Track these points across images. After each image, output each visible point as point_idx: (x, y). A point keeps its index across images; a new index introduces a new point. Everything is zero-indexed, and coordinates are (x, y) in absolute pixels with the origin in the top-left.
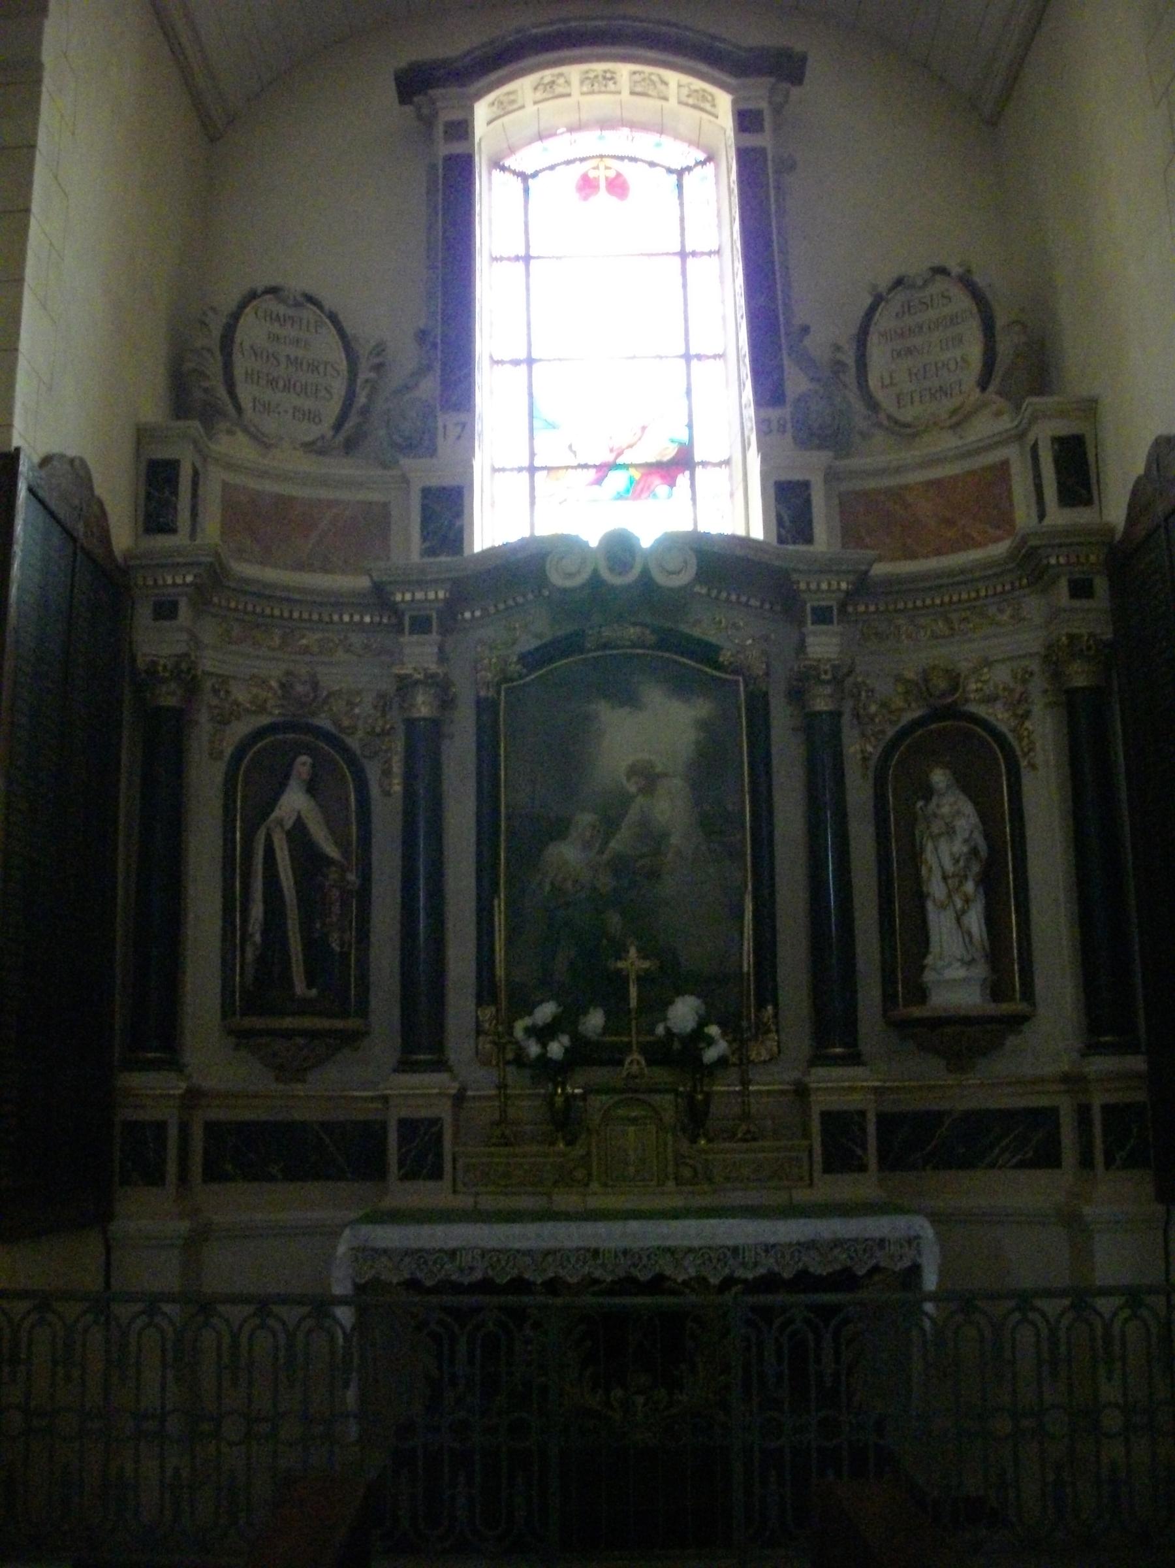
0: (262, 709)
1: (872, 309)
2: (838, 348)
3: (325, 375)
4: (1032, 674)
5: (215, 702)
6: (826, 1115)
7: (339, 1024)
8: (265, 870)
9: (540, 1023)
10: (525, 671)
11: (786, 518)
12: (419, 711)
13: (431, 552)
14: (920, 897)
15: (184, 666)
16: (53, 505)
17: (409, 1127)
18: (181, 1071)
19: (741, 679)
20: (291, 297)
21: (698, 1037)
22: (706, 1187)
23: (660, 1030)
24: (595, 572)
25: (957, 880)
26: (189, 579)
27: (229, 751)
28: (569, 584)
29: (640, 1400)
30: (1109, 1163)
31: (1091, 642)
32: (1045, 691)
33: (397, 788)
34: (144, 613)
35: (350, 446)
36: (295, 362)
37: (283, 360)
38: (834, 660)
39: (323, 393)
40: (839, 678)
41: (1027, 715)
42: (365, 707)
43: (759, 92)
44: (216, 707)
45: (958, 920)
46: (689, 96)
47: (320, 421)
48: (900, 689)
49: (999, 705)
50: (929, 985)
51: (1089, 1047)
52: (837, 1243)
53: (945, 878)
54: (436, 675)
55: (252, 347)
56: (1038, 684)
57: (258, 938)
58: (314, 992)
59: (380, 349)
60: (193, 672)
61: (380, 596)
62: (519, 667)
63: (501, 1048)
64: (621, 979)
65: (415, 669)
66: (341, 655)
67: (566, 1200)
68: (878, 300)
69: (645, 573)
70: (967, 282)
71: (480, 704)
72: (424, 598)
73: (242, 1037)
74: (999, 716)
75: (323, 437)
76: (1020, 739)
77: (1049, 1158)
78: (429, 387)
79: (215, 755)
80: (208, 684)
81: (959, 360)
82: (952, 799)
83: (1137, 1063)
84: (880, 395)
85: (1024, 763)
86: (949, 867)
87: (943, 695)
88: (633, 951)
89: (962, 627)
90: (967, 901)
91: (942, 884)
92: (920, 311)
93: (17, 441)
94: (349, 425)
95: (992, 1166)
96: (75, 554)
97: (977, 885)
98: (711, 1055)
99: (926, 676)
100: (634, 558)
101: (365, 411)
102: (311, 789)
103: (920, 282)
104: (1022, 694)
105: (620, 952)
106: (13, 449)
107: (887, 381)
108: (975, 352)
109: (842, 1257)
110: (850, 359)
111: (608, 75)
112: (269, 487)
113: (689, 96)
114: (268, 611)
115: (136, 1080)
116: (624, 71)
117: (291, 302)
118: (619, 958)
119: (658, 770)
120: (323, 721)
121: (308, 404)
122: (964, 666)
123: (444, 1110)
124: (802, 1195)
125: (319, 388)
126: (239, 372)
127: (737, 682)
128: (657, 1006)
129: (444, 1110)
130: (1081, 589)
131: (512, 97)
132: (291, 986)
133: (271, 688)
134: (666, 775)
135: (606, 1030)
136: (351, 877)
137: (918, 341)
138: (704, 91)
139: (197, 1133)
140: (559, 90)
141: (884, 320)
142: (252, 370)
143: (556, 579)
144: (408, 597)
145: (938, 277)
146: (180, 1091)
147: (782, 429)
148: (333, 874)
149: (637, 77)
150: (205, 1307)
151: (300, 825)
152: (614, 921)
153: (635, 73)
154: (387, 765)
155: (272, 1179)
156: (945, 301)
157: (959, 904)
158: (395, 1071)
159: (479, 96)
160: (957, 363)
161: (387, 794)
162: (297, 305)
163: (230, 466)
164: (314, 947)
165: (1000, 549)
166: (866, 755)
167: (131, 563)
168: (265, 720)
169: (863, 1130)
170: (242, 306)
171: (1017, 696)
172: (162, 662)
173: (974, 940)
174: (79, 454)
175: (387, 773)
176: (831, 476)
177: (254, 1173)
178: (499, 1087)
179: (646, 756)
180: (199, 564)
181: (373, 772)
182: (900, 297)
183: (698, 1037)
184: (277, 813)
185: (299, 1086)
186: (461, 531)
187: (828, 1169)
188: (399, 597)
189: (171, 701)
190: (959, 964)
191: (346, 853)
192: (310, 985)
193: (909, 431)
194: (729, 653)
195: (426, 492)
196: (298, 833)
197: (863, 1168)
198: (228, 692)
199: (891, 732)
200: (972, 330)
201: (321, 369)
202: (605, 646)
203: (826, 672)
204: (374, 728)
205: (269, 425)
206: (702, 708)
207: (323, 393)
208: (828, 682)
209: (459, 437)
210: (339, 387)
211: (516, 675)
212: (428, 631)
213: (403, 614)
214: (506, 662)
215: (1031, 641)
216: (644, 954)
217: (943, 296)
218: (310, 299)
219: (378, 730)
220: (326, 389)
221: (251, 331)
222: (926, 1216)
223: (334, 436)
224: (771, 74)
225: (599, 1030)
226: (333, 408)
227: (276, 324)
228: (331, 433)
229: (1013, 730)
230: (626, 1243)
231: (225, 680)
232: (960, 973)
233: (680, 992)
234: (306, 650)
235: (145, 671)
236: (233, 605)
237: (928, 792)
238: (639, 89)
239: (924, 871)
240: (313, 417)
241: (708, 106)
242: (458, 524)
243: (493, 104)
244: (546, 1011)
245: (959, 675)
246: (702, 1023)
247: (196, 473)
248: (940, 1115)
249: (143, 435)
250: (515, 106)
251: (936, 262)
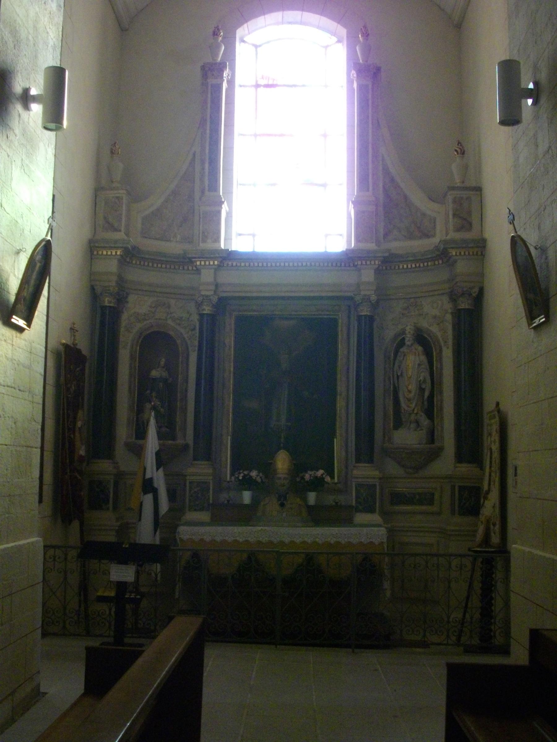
123: (180, 441)
233: (322, 469)
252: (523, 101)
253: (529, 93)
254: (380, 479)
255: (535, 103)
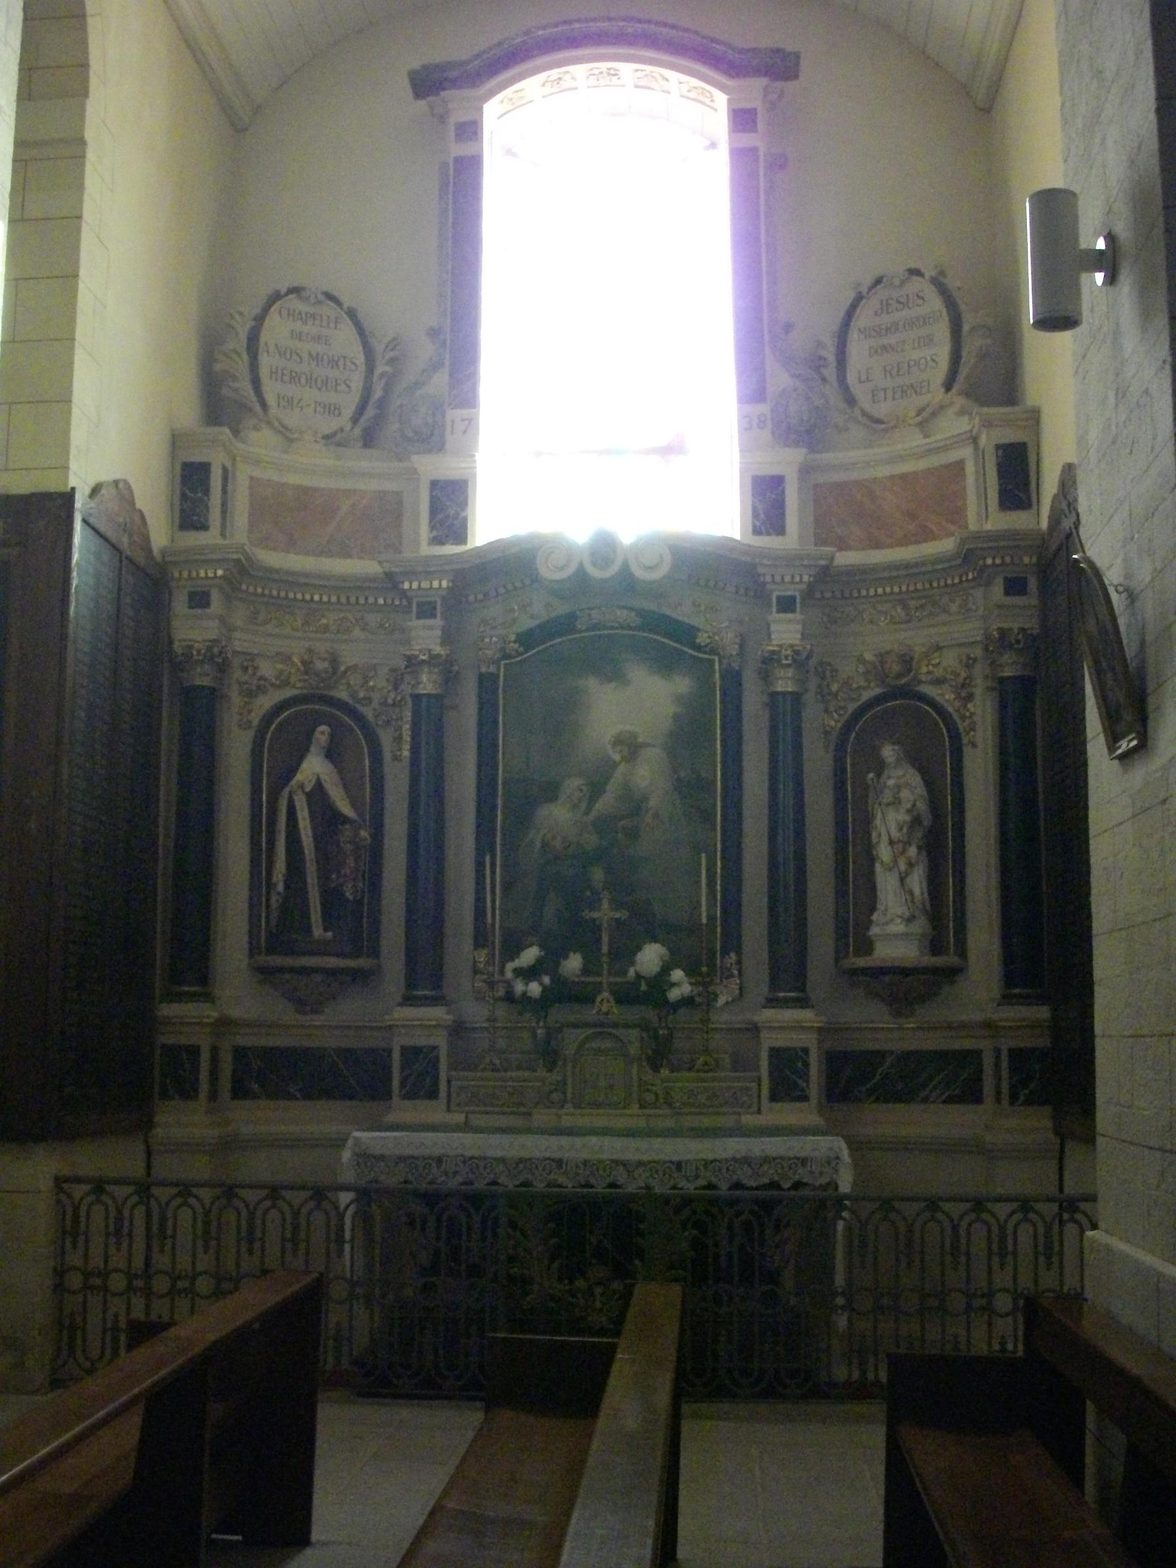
0: (286, 683)
1: (854, 307)
2: (820, 344)
3: (344, 368)
4: (975, 660)
5: (245, 678)
6: (775, 1053)
7: (351, 963)
8: (288, 825)
9: (525, 965)
10: (521, 649)
11: (761, 512)
12: (425, 688)
13: (438, 541)
14: (872, 860)
15: (216, 650)
16: (102, 529)
17: (411, 1054)
18: (213, 1002)
19: (716, 658)
20: (313, 296)
21: (660, 981)
22: (668, 1111)
23: (631, 972)
24: (581, 565)
25: (901, 845)
26: (220, 572)
27: (256, 722)
28: (558, 576)
29: (598, 1290)
30: (1013, 1098)
31: (1020, 636)
32: (986, 677)
33: (406, 753)
34: (180, 604)
35: (369, 439)
36: (317, 358)
37: (305, 356)
38: (798, 646)
39: (343, 387)
40: (800, 662)
41: (970, 697)
42: (380, 682)
43: (754, 88)
44: (246, 683)
45: (902, 880)
46: (689, 91)
47: (340, 414)
48: (861, 669)
49: (946, 687)
50: (874, 938)
51: (1004, 997)
52: (766, 1160)
53: (891, 843)
54: (439, 656)
55: (276, 345)
56: (979, 671)
57: (281, 887)
58: (330, 934)
59: (394, 343)
60: (224, 655)
61: (391, 581)
62: (516, 646)
63: (491, 985)
64: (595, 928)
65: (420, 651)
66: (357, 632)
67: (542, 1117)
68: (859, 298)
69: (625, 567)
70: (939, 284)
71: (482, 678)
72: (428, 586)
73: (265, 974)
74: (945, 696)
75: (342, 430)
76: (963, 718)
77: (971, 1094)
78: (440, 381)
79: (246, 726)
80: (236, 662)
81: (929, 358)
82: (901, 772)
83: (1043, 1013)
84: (857, 390)
85: (965, 740)
86: (895, 834)
87: (899, 676)
88: (605, 905)
89: (917, 614)
90: (911, 865)
91: (889, 848)
92: (897, 310)
93: (73, 482)
94: (370, 412)
95: (925, 1100)
96: (121, 561)
97: (919, 848)
98: (674, 994)
99: (882, 656)
100: (614, 552)
101: (382, 404)
102: (332, 754)
103: (897, 282)
104: (965, 679)
105: (594, 904)
106: (69, 490)
107: (863, 378)
108: (943, 353)
109: (769, 1173)
110: (830, 355)
111: (612, 72)
112: (293, 479)
113: (689, 91)
114: (291, 595)
115: (168, 1010)
116: (626, 69)
117: (312, 300)
118: (592, 909)
119: (640, 740)
120: (342, 694)
121: (331, 397)
122: (919, 650)
123: (440, 1040)
124: (749, 1119)
125: (339, 381)
126: (264, 372)
127: (711, 662)
128: (625, 953)
129: (440, 1040)
130: (1015, 586)
131: (520, 94)
132: (308, 929)
133: (294, 664)
134: (647, 745)
135: (585, 971)
136: (364, 834)
137: (892, 340)
138: (704, 89)
139: (227, 1058)
140: (565, 84)
141: (863, 318)
142: (277, 368)
143: (547, 572)
144: (415, 585)
145: (914, 278)
146: (212, 1020)
147: (762, 423)
148: (347, 832)
149: (640, 74)
150: (230, 1191)
151: (319, 785)
152: (597, 875)
153: (637, 70)
154: (398, 733)
155: (291, 1097)
156: (920, 302)
157: (903, 866)
158: (401, 1005)
159: (492, 93)
160: (927, 362)
161: (396, 758)
162: (319, 302)
163: (257, 462)
164: (332, 898)
165: (945, 546)
166: (828, 729)
167: (168, 559)
168: (288, 693)
169: (806, 1065)
170: (266, 309)
171: (961, 680)
172: (196, 645)
173: (916, 900)
174: (123, 477)
175: (399, 739)
176: (806, 470)
177: (277, 1093)
178: (488, 1020)
179: (628, 727)
180: (228, 560)
181: (386, 738)
182: (882, 293)
183: (660, 981)
184: (299, 777)
185: (315, 1017)
186: (465, 520)
187: (774, 1098)
188: (406, 586)
189: (206, 682)
190: (899, 920)
191: (361, 814)
192: (326, 930)
193: (883, 426)
194: (706, 635)
195: (434, 484)
196: (318, 794)
197: (804, 1098)
198: (256, 668)
199: (852, 707)
200: (942, 331)
201: (341, 363)
202: (594, 627)
203: (786, 657)
204: (386, 700)
205: (292, 419)
206: (682, 684)
207: (343, 387)
208: (789, 666)
209: (465, 432)
210: (357, 381)
211: (513, 653)
212: (433, 616)
213: (412, 599)
214: (505, 641)
215: (971, 629)
216: (617, 905)
217: (918, 296)
218: (330, 297)
219: (390, 701)
220: (345, 382)
221: (276, 330)
222: (843, 1137)
223: (352, 428)
224: (766, 74)
225: (578, 972)
226: (349, 405)
227: (299, 323)
228: (349, 426)
229: (958, 711)
230: (585, 1155)
231: (252, 657)
232: (899, 927)
233: (655, 939)
234: (326, 629)
235: (183, 654)
236: (259, 590)
237: (880, 767)
238: (641, 83)
239: (874, 835)
240: (333, 410)
241: (707, 101)
242: (463, 514)
243: (502, 102)
244: (530, 955)
245: (912, 658)
246: (666, 970)
247: (225, 470)
248: (882, 1054)
249: (176, 440)
250: (524, 102)
251: (913, 266)
252: (1084, 276)
253: (1098, 260)
254: (820, 1030)
255: (1111, 279)
